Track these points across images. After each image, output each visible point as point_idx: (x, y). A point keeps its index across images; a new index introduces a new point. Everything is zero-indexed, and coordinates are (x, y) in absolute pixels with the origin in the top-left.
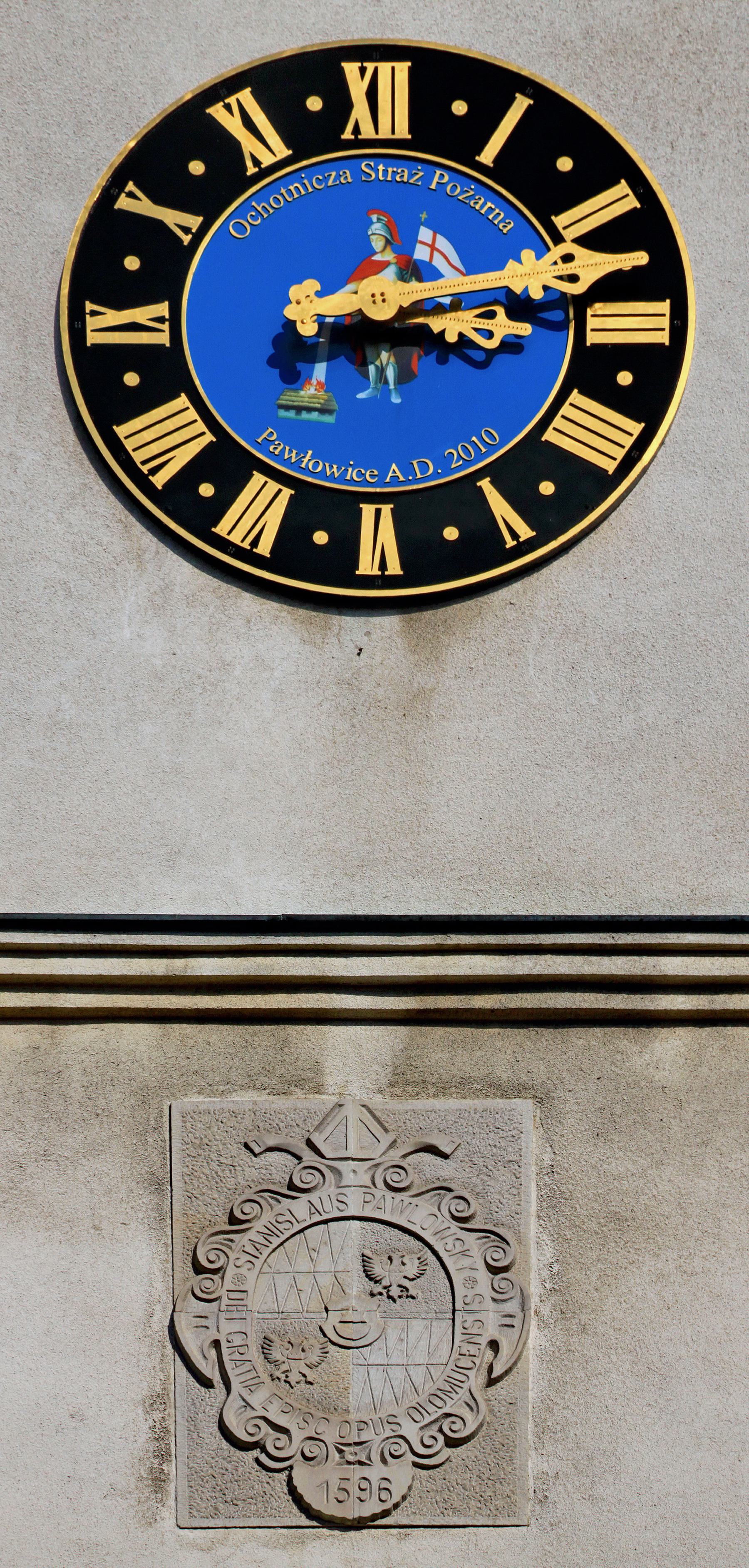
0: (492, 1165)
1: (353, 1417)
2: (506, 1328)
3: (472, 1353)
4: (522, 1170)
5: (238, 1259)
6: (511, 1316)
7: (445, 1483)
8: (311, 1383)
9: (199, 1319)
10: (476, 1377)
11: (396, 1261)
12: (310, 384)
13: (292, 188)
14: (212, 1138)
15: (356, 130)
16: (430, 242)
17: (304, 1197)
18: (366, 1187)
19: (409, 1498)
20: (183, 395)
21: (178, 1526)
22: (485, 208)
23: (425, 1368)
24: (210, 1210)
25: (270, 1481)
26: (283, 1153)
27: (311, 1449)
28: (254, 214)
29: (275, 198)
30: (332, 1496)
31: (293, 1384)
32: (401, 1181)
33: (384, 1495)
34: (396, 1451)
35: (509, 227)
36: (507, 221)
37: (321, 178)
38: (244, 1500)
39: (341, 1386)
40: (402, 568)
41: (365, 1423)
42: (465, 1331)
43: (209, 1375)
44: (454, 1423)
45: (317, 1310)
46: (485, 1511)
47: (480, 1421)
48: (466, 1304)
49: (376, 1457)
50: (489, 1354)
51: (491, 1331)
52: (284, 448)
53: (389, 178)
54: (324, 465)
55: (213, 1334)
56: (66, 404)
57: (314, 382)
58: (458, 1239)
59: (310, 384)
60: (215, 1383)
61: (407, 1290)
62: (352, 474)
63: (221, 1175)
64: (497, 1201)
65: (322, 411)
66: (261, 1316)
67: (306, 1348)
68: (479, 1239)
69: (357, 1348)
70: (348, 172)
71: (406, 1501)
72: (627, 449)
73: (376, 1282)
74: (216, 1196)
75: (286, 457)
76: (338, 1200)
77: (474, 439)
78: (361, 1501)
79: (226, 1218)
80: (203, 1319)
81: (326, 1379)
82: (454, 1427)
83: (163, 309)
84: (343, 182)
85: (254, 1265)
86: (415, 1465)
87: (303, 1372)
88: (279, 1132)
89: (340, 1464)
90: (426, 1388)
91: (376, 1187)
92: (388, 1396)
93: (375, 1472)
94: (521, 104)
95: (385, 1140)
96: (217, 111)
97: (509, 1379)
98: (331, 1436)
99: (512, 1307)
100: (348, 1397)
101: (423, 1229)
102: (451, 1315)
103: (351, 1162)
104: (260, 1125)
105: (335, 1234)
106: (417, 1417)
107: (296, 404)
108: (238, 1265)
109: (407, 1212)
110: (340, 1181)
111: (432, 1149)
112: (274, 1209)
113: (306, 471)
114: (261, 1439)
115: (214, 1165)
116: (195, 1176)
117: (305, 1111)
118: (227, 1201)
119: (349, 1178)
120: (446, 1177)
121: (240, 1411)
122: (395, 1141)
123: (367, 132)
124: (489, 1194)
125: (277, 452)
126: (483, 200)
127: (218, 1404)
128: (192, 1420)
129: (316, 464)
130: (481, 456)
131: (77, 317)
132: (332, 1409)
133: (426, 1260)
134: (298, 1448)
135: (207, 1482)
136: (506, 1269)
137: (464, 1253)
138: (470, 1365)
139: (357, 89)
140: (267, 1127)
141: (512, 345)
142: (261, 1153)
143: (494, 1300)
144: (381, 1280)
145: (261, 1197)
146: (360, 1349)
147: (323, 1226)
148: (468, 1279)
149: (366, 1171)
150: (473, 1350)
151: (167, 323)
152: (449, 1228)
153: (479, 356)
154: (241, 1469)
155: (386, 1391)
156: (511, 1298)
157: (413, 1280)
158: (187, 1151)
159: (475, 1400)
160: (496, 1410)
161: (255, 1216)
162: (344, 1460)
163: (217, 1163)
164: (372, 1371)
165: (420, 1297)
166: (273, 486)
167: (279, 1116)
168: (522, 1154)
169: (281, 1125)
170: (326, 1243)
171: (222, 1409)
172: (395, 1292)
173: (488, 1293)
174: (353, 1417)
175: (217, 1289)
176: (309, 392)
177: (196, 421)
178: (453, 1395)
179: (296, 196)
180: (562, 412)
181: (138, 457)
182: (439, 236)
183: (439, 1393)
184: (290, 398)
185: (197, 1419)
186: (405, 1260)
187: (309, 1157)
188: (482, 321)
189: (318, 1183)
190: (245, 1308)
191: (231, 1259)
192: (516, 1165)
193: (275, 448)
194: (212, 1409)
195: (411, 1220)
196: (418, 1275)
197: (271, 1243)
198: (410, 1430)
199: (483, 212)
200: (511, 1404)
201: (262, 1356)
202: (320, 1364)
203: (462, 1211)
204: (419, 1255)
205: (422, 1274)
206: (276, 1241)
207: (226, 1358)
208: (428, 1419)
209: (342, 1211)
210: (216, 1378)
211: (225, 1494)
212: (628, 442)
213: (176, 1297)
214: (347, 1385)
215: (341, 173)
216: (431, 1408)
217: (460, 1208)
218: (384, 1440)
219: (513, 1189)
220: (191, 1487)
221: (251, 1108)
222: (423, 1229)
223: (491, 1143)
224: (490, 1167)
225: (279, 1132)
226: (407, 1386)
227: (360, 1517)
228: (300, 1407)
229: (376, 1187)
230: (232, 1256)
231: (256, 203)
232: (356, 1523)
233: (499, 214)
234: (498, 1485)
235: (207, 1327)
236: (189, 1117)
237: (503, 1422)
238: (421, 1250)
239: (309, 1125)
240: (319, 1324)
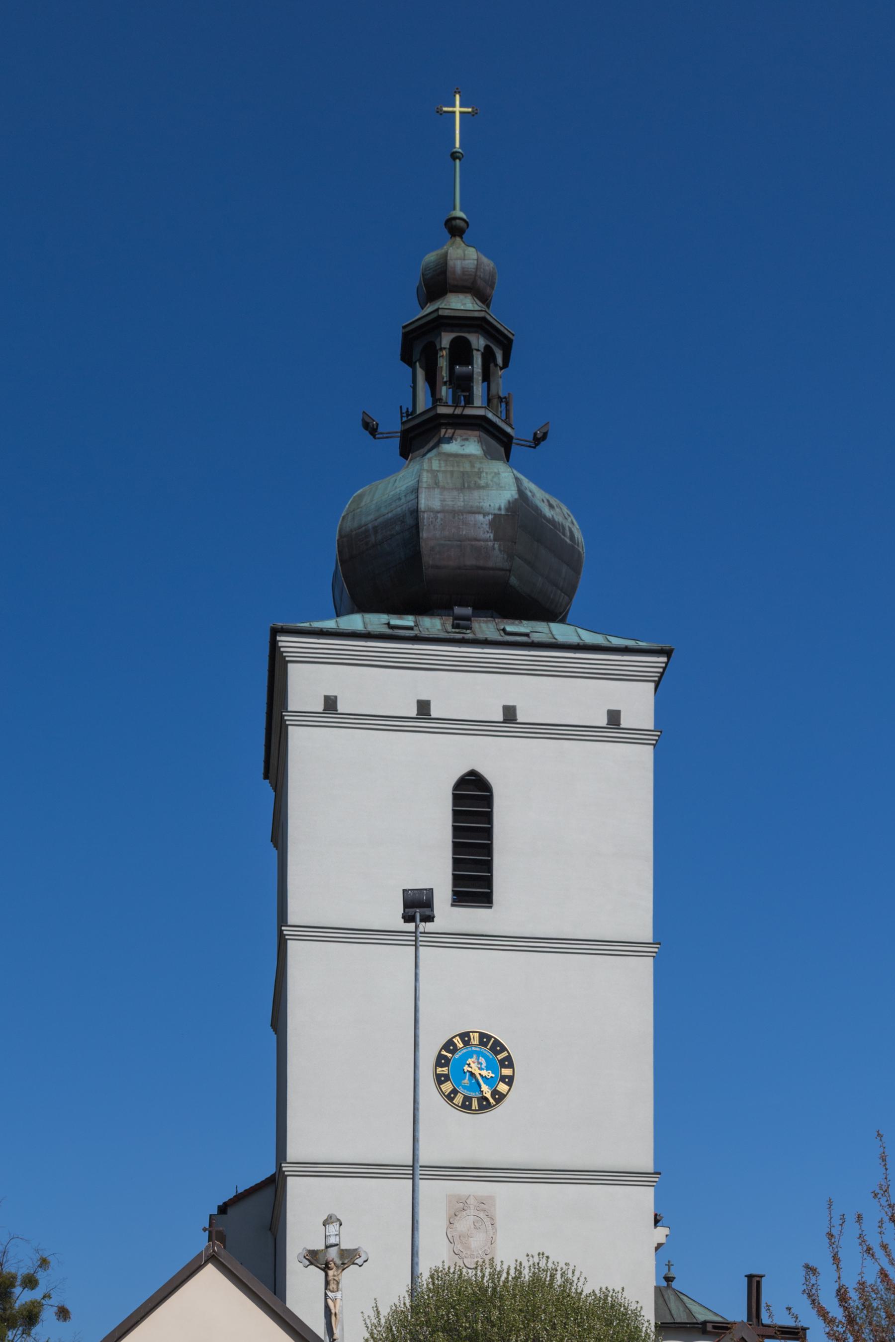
51: (491, 1235)
55: (452, 1235)
65: (468, 1084)
83: (447, 1068)
98: (469, 1253)
111: (483, 1203)
119: (471, 1209)
131: (436, 1069)
139: (472, 1037)
198: (480, 1252)
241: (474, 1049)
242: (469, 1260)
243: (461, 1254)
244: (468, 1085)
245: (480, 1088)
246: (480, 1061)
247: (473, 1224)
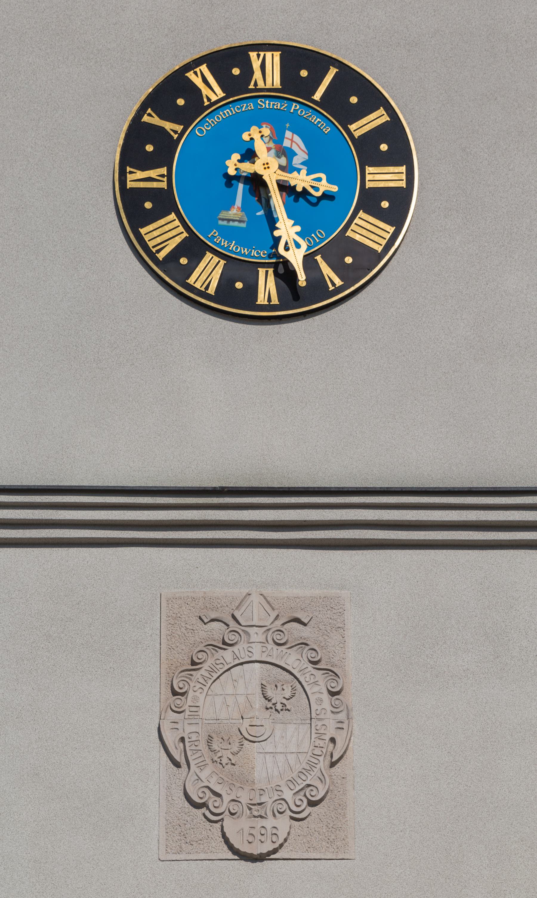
0: (329, 630)
1: (257, 786)
2: (339, 730)
3: (321, 746)
4: (345, 632)
5: (195, 686)
6: (342, 722)
7: (308, 830)
8: (234, 765)
9: (173, 724)
10: (324, 761)
11: (279, 688)
12: (234, 208)
13: (225, 112)
14: (182, 613)
15: (256, 84)
16: (291, 138)
17: (230, 649)
18: (263, 643)
19: (288, 840)
20: (173, 213)
21: (159, 859)
22: (316, 122)
23: (296, 755)
24: (180, 656)
25: (211, 828)
26: (219, 623)
27: (234, 808)
28: (207, 124)
29: (217, 117)
30: (245, 839)
31: (224, 765)
32: (282, 639)
33: (274, 838)
34: (280, 809)
35: (328, 130)
36: (327, 128)
37: (239, 107)
38: (196, 842)
39: (251, 766)
40: (279, 301)
41: (264, 790)
42: (317, 732)
43: (178, 760)
44: (312, 790)
45: (237, 718)
46: (331, 850)
47: (326, 789)
48: (317, 715)
49: (270, 813)
50: (331, 745)
51: (331, 732)
52: (221, 240)
53: (271, 107)
54: (241, 248)
56: (135, 255)
57: (236, 207)
58: (312, 674)
59: (234, 208)
60: (181, 764)
61: (286, 706)
62: (254, 253)
63: (187, 635)
64: (333, 651)
65: (240, 221)
66: (207, 722)
67: (231, 742)
68: (323, 674)
69: (259, 742)
70: (251, 104)
71: (287, 843)
72: (387, 240)
73: (269, 701)
74: (184, 648)
75: (222, 244)
76: (248, 651)
77: (313, 235)
78: (262, 842)
79: (189, 662)
80: (175, 724)
81: (242, 762)
82: (313, 794)
83: (164, 171)
84: (250, 109)
85: (203, 690)
86: (292, 818)
87: (230, 758)
88: (218, 610)
89: (250, 818)
90: (297, 767)
91: (268, 643)
92: (276, 773)
93: (269, 823)
94: (332, 72)
95: (273, 615)
96: (191, 75)
97: (342, 761)
98: (244, 800)
99: (342, 716)
100: (254, 774)
101: (294, 668)
102: (310, 721)
103: (255, 628)
104: (207, 606)
105: (247, 671)
106: (292, 787)
107: (227, 218)
108: (195, 690)
109: (285, 658)
110: (249, 639)
112: (214, 656)
113: (231, 251)
114: (206, 801)
115: (183, 629)
116: (173, 636)
117: (231, 598)
118: (190, 651)
119: (254, 638)
120: (306, 637)
121: (195, 783)
122: (278, 616)
123: (261, 85)
124: (328, 647)
125: (218, 242)
126: (315, 117)
127: (183, 778)
128: (168, 788)
129: (237, 248)
130: (317, 244)
132: (246, 781)
133: (295, 687)
134: (227, 807)
135: (176, 829)
136: (338, 693)
137: (316, 683)
138: (320, 753)
139: (256, 64)
140: (212, 607)
141: (327, 196)
142: (208, 622)
143: (332, 712)
144: (271, 699)
145: (208, 649)
146: (261, 743)
147: (240, 667)
148: (318, 699)
149: (263, 634)
150: (322, 743)
151: (166, 178)
152: (307, 668)
153: (314, 200)
154: (195, 821)
155: (275, 770)
156: (341, 711)
157: (288, 699)
158: (169, 621)
159: (323, 775)
160: (335, 782)
161: (205, 661)
162: (252, 815)
163: (185, 628)
164: (268, 756)
165: (292, 710)
166: (216, 259)
167: (217, 600)
168: (345, 623)
169: (219, 606)
170: (241, 677)
171: (185, 781)
172: (279, 707)
173: (329, 708)
174: (257, 786)
175: (183, 705)
176: (233, 212)
177: (179, 226)
178: (311, 772)
179: (227, 116)
180: (355, 221)
181: (151, 244)
182: (295, 135)
183: (304, 771)
184: (224, 215)
185: (171, 788)
186: (284, 687)
187: (233, 625)
188: (315, 182)
189: (238, 641)
190: (198, 717)
191: (191, 687)
192: (342, 629)
193: (217, 240)
194: (179, 781)
195: (287, 663)
196: (291, 696)
197: (212, 676)
198: (288, 795)
199: (315, 123)
200: (343, 778)
201: (207, 747)
202: (239, 752)
203: (314, 658)
204: (291, 685)
205: (294, 696)
206: (215, 676)
207: (188, 749)
208: (298, 788)
209: (250, 657)
210: (183, 762)
211: (186, 838)
212: (388, 236)
213: (161, 710)
214: (253, 766)
215: (249, 105)
216: (299, 781)
217: (313, 656)
218: (274, 802)
219: (341, 644)
220: (167, 833)
221: (203, 595)
222: (294, 668)
223: (329, 616)
224: (328, 631)
225: (218, 610)
226: (286, 766)
227: (261, 853)
228: (228, 780)
229: (268, 643)
230: (192, 684)
231: (209, 119)
232: (259, 857)
233: (323, 124)
234: (337, 832)
235: (177, 729)
236: (170, 601)
237: (339, 790)
238: (293, 681)
239: (233, 605)
240: (238, 726)
241: (267, 104)
242: (244, 823)
243: (212, 802)
244: (243, 225)
245: (273, 228)
246: (286, 143)
247: (259, 690)
